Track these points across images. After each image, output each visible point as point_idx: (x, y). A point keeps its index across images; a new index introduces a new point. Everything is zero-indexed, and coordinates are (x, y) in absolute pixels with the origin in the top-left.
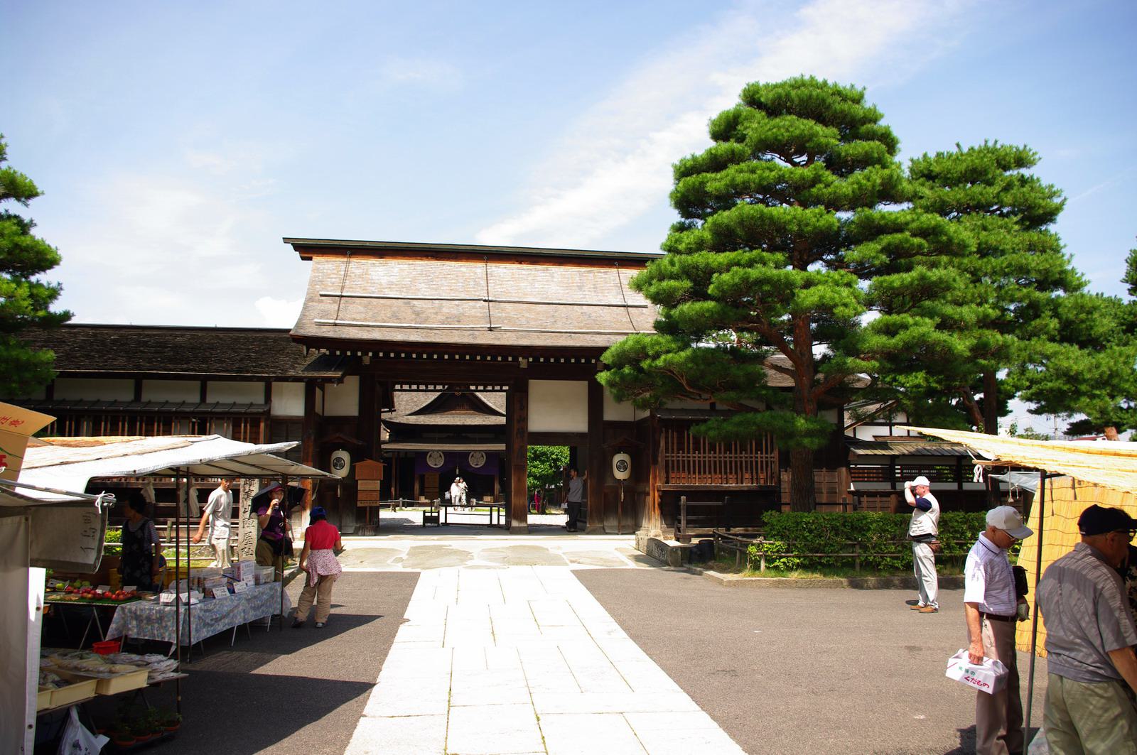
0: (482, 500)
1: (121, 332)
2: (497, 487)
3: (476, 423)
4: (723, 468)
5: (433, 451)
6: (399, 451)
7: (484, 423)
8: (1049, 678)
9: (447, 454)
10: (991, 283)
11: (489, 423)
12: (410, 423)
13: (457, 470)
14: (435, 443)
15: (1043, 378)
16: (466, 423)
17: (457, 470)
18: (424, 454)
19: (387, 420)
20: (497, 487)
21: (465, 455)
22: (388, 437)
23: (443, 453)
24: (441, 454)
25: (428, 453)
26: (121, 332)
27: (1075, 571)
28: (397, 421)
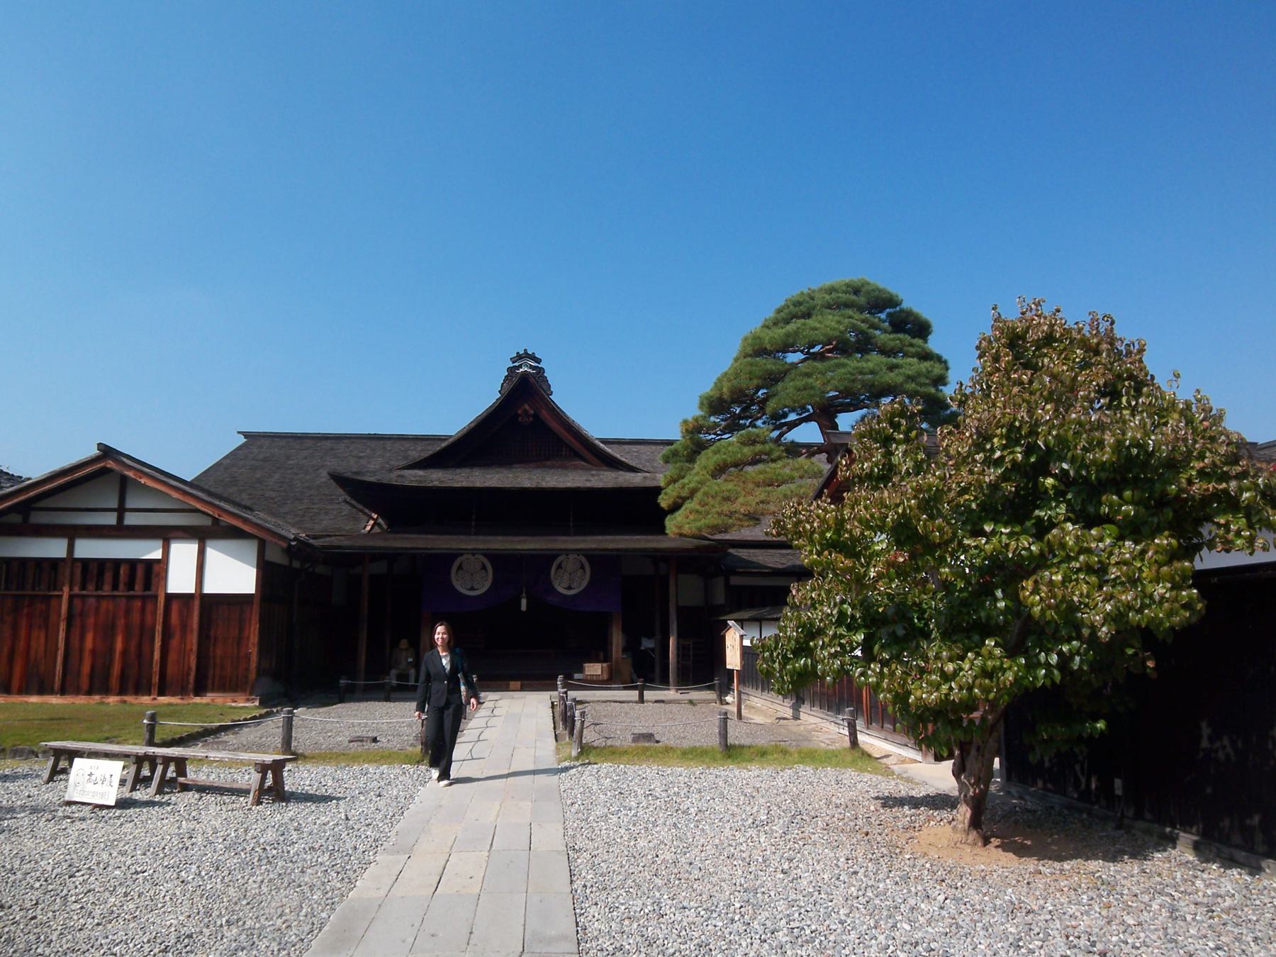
0: (572, 679)
1: (548, 417)
2: (617, 639)
3: (569, 485)
4: (222, 504)
5: (567, 552)
7: (588, 485)
8: (1237, 847)
9: (497, 559)
10: (959, 406)
11: (601, 485)
12: (407, 483)
13: (524, 602)
14: (569, 535)
15: (852, 337)
16: (544, 485)
17: (524, 602)
18: (447, 559)
20: (617, 639)
21: (544, 561)
23: (587, 557)
24: (584, 560)
25: (556, 556)
26: (548, 417)
27: (1139, 626)
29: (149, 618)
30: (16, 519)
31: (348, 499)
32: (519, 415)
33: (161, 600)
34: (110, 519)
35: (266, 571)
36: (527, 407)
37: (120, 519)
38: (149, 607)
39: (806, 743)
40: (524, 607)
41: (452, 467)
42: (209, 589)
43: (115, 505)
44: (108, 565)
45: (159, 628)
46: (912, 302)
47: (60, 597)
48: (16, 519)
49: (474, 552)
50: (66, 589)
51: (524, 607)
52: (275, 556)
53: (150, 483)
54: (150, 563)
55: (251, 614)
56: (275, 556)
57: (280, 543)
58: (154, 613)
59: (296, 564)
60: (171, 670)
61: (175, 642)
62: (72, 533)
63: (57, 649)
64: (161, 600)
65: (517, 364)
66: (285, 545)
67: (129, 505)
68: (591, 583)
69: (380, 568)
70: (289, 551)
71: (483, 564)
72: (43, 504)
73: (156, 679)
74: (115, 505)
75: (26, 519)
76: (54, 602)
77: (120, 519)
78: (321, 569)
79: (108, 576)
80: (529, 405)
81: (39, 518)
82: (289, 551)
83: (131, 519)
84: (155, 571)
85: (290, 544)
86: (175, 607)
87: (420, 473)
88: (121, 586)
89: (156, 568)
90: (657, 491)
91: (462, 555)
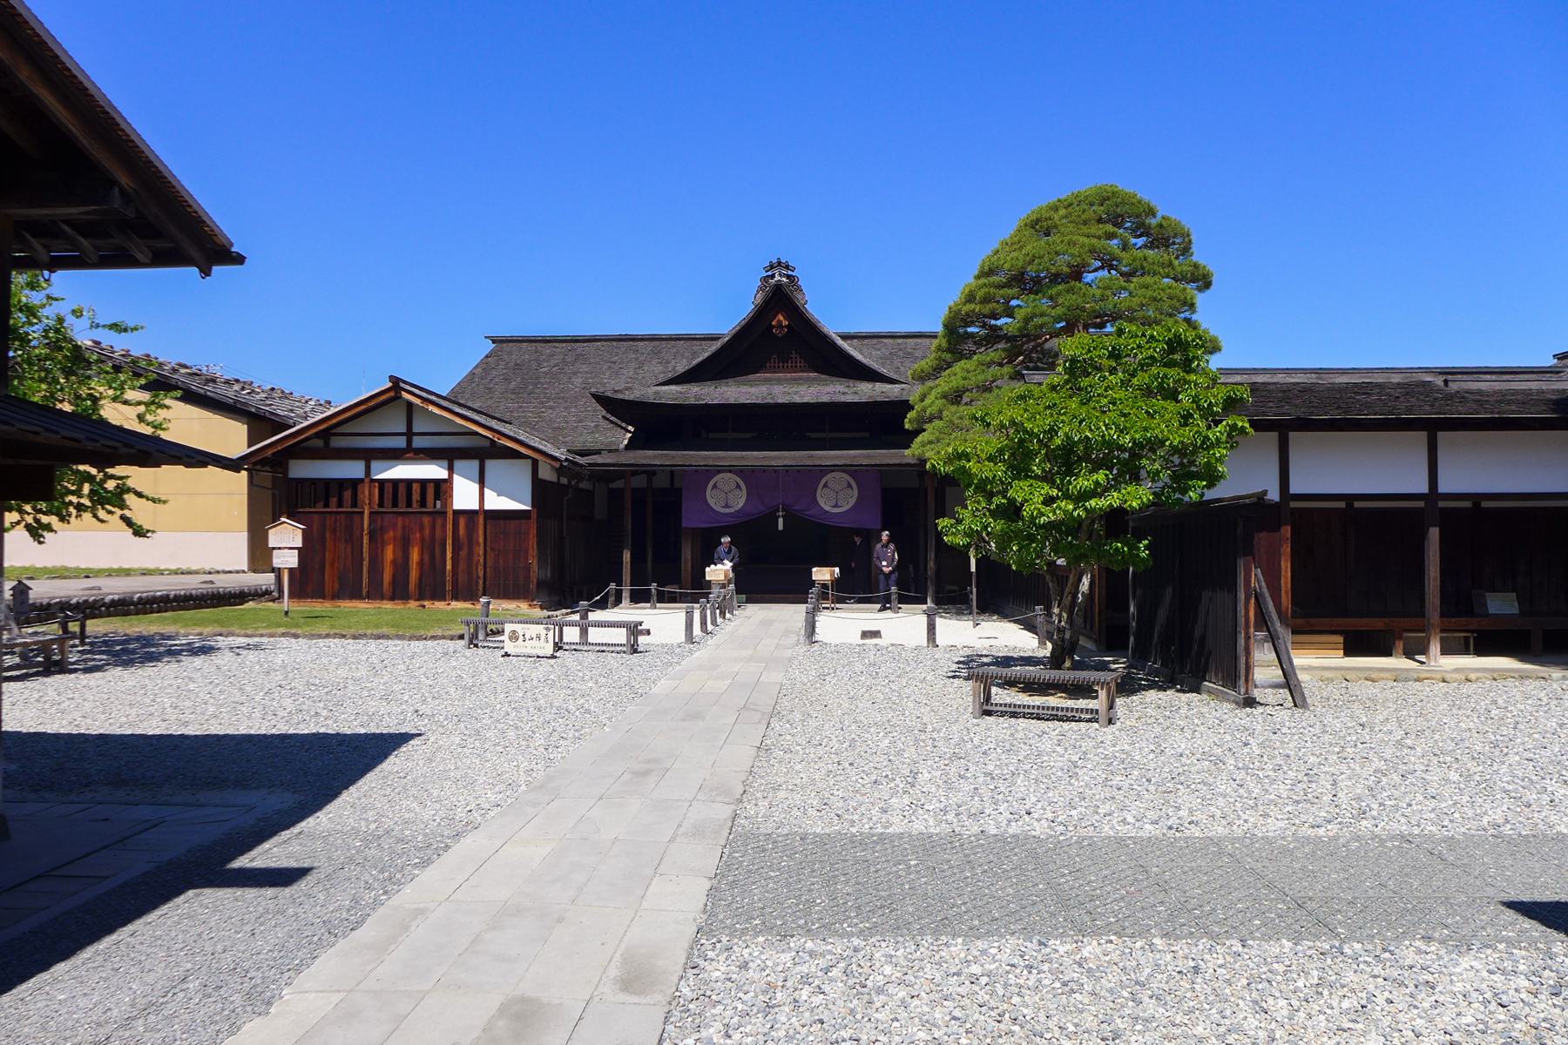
5: (719, 470)
6: (650, 472)
11: (856, 399)
13: (781, 521)
17: (781, 521)
19: (609, 394)
21: (811, 477)
22: (626, 442)
28: (631, 397)
29: (438, 532)
30: (319, 443)
31: (609, 416)
32: (774, 327)
33: (450, 516)
34: (401, 442)
35: (540, 489)
36: (781, 318)
37: (409, 442)
38: (439, 522)
39: (22, 317)
40: (781, 527)
41: (711, 379)
42: (487, 507)
43: (415, 438)
44: (402, 489)
45: (449, 542)
46: (1168, 207)
47: (363, 513)
48: (319, 443)
49: (730, 469)
50: (366, 507)
51: (781, 527)
52: (546, 473)
53: (436, 410)
54: (438, 483)
55: (176, 645)
56: (546, 473)
57: (553, 463)
58: (444, 526)
59: (564, 481)
60: (462, 578)
61: (463, 553)
62: (369, 455)
63: (362, 560)
64: (450, 516)
65: (770, 273)
66: (557, 465)
67: (415, 430)
68: (857, 503)
69: (639, 482)
70: (561, 471)
71: (712, 489)
72: (334, 431)
73: (449, 587)
74: (415, 438)
75: (327, 443)
76: (356, 518)
77: (409, 442)
78: (585, 485)
79: (348, 494)
80: (783, 316)
81: (337, 442)
82: (561, 471)
83: (418, 442)
84: (441, 489)
85: (561, 464)
86: (462, 522)
87: (673, 387)
88: (415, 505)
89: (443, 487)
90: (906, 406)
91: (719, 472)
